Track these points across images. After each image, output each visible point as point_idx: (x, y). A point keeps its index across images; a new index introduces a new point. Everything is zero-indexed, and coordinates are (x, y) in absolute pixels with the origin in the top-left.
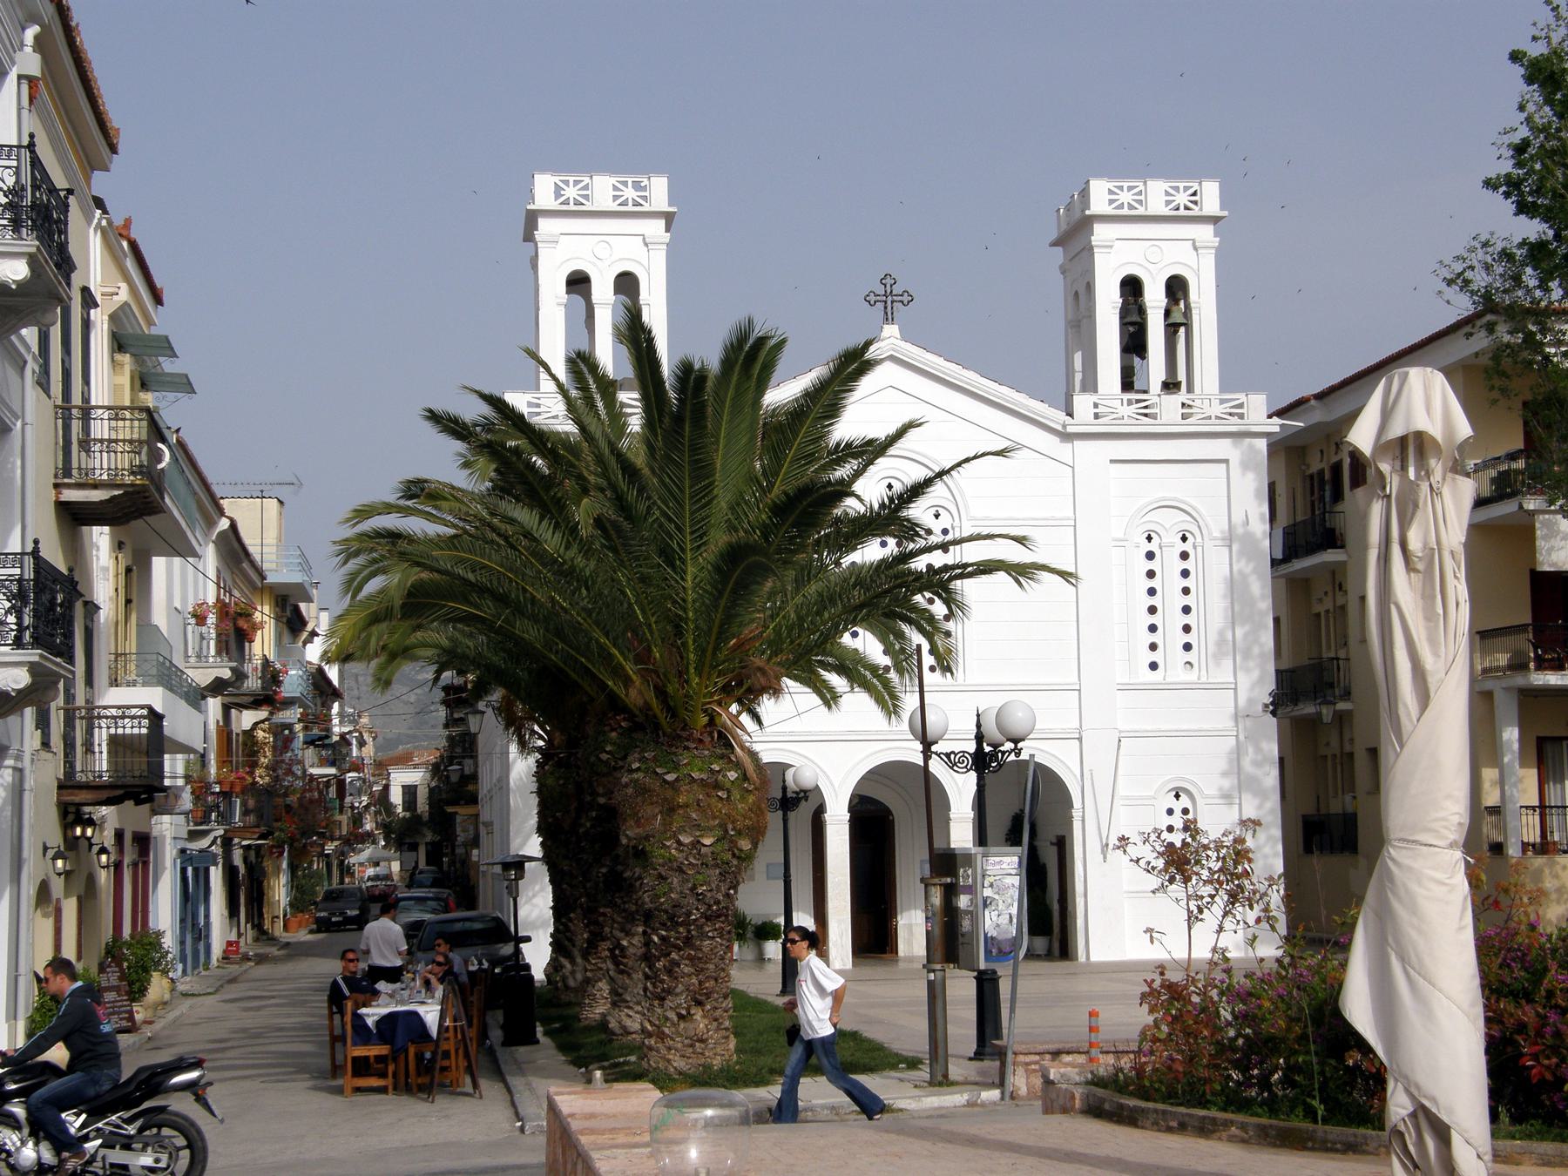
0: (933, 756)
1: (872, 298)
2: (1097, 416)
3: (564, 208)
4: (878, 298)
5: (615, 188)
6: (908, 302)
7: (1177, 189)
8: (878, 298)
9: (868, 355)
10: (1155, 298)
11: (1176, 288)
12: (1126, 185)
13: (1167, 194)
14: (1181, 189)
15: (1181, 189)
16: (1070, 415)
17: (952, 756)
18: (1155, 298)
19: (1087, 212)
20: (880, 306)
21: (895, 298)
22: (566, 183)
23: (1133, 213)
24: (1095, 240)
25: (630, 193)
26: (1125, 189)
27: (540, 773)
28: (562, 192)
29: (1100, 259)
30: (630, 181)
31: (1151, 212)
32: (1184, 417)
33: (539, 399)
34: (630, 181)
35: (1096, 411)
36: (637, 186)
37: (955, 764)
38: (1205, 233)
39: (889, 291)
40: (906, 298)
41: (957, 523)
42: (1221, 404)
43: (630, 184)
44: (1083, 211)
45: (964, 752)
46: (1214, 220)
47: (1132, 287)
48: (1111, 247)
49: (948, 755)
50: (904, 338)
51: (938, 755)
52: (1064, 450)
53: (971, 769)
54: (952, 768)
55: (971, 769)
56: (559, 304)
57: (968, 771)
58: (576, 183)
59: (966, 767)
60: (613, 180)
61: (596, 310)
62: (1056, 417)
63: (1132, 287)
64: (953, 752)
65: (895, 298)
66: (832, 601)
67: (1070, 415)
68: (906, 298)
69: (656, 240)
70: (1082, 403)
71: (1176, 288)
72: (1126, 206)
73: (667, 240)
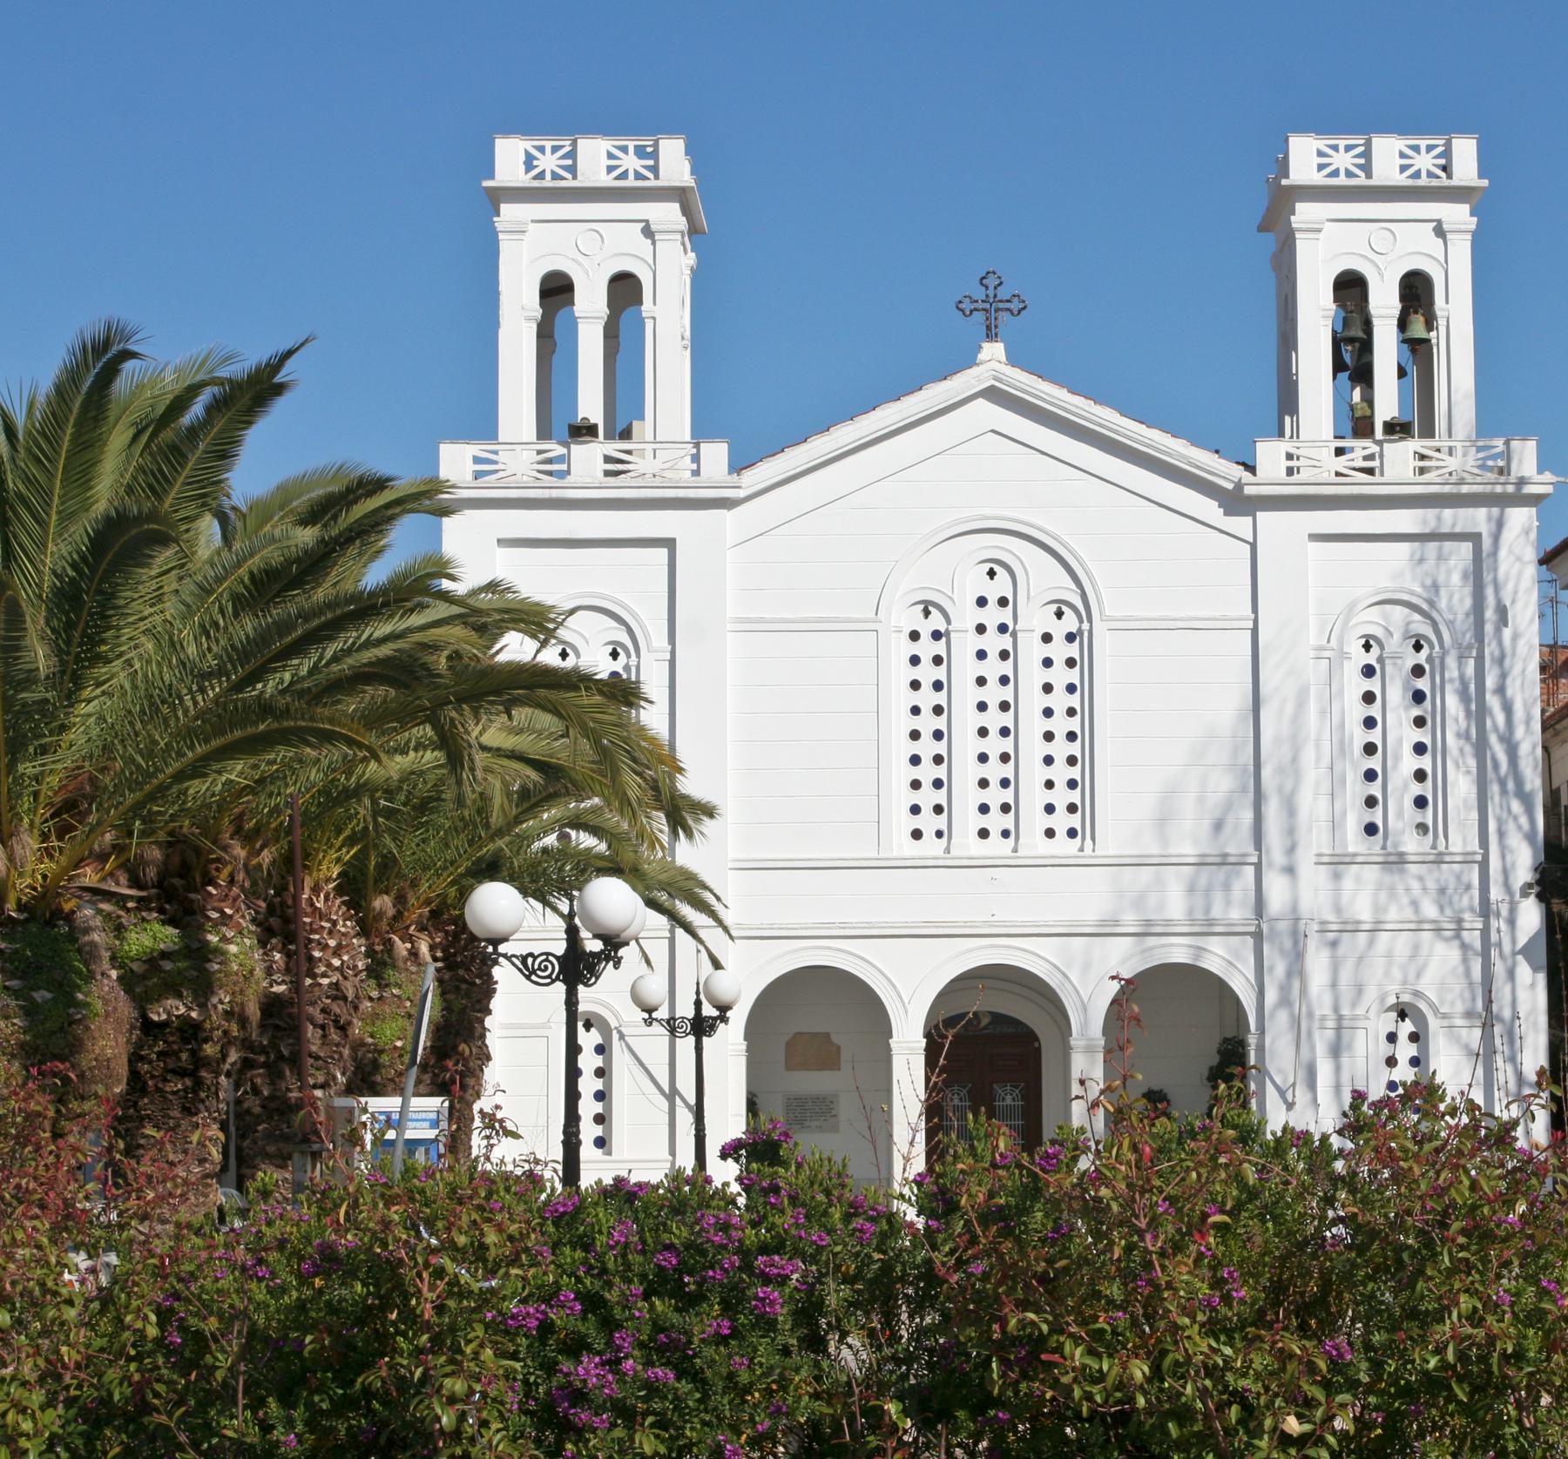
0: (501, 959)
1: (967, 306)
2: (1290, 471)
3: (536, 184)
4: (976, 305)
5: (610, 156)
6: (962, 310)
7: (1416, 149)
8: (976, 305)
9: (278, 379)
10: (1384, 303)
11: (1416, 291)
12: (1342, 144)
13: (1402, 155)
14: (1423, 150)
15: (1423, 150)
16: (1251, 469)
17: (530, 960)
18: (1384, 303)
19: (1284, 182)
20: (979, 317)
21: (1001, 305)
22: (541, 149)
23: (1435, 183)
24: (1296, 221)
25: (631, 162)
26: (1342, 149)
27: (609, 1025)
28: (535, 163)
29: (1304, 249)
30: (631, 145)
31: (583, 181)
32: (1422, 471)
33: (496, 453)
34: (631, 145)
35: (1290, 463)
36: (640, 152)
37: (534, 972)
38: (1458, 215)
39: (992, 295)
40: (1015, 306)
41: (1086, 626)
42: (1478, 452)
43: (631, 150)
44: (1277, 179)
45: (548, 954)
46: (679, 195)
47: (1350, 287)
48: (1319, 230)
49: (524, 959)
50: (1013, 360)
51: (508, 958)
52: (1242, 525)
53: (557, 978)
54: (528, 978)
55: (557, 978)
56: (529, 319)
57: (553, 981)
58: (555, 149)
59: (549, 976)
60: (1321, 143)
61: (580, 326)
62: (1226, 472)
63: (1350, 287)
64: (531, 955)
65: (1001, 305)
66: (651, 744)
67: (1251, 469)
68: (1015, 306)
69: (666, 228)
70: (1271, 455)
71: (1416, 291)
72: (1342, 172)
73: (1473, 227)
